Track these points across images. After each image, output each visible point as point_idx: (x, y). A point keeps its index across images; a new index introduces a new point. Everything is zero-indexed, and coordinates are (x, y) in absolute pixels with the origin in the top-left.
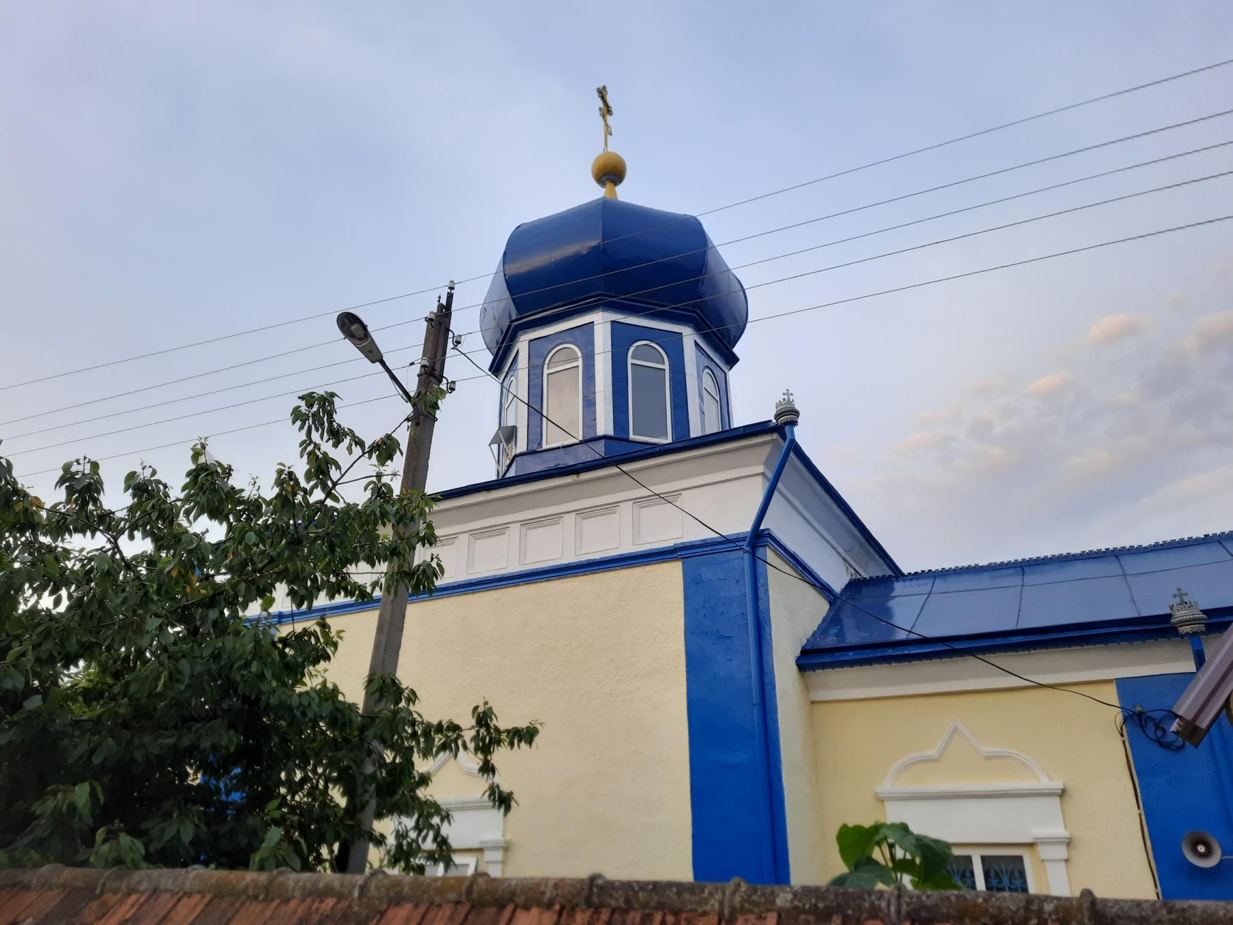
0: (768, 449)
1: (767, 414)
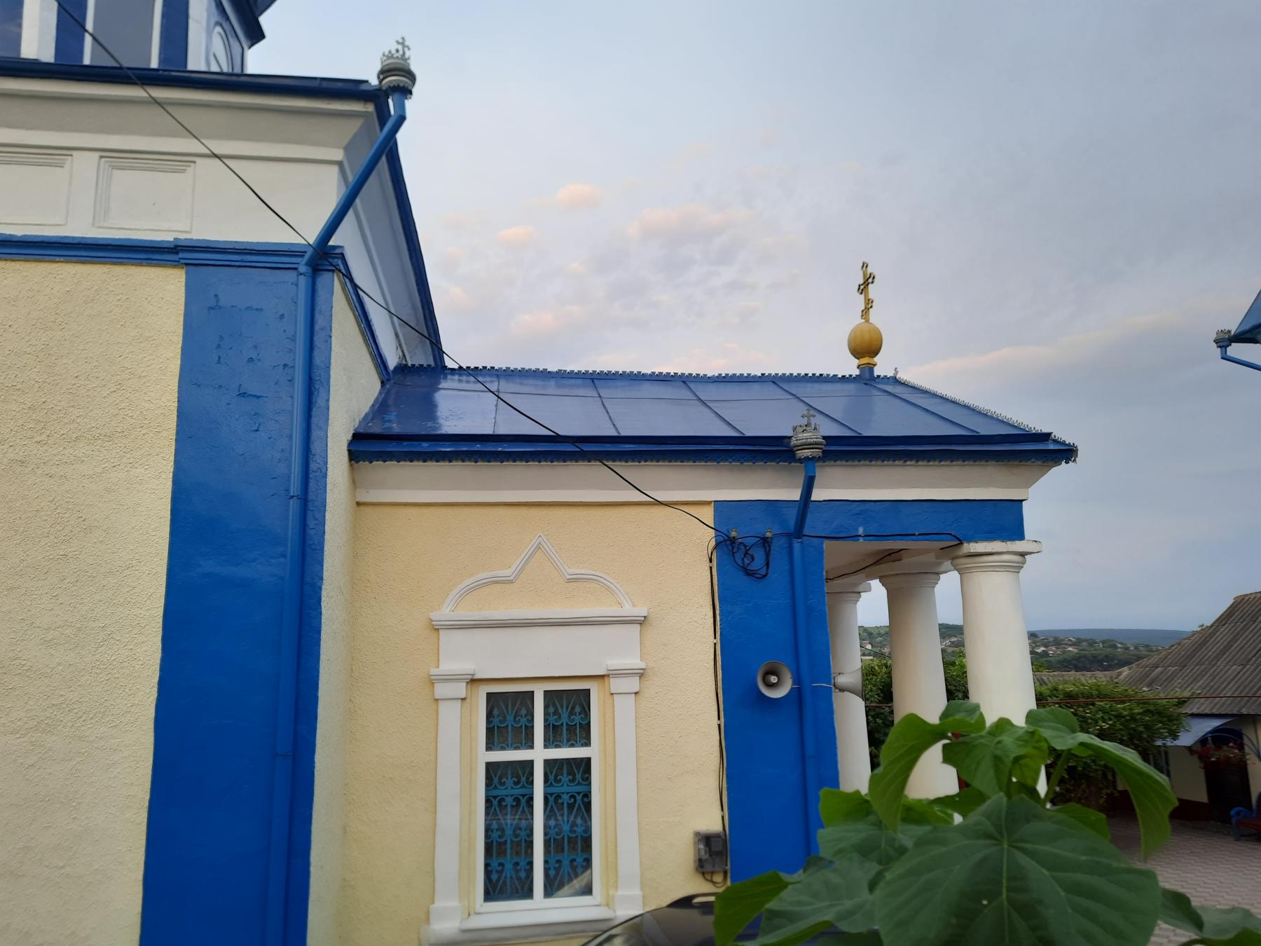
0: (354, 126)
1: (365, 68)
